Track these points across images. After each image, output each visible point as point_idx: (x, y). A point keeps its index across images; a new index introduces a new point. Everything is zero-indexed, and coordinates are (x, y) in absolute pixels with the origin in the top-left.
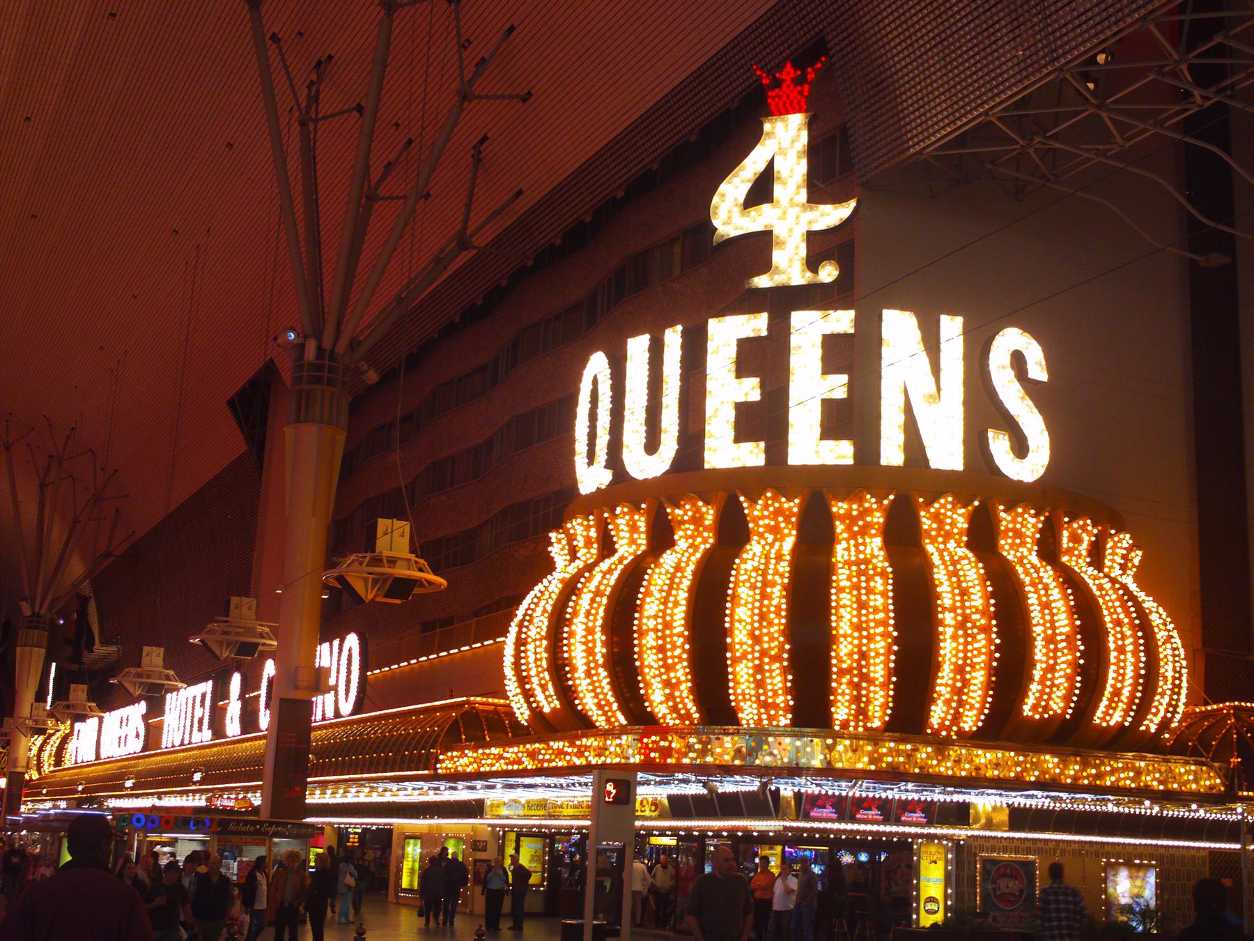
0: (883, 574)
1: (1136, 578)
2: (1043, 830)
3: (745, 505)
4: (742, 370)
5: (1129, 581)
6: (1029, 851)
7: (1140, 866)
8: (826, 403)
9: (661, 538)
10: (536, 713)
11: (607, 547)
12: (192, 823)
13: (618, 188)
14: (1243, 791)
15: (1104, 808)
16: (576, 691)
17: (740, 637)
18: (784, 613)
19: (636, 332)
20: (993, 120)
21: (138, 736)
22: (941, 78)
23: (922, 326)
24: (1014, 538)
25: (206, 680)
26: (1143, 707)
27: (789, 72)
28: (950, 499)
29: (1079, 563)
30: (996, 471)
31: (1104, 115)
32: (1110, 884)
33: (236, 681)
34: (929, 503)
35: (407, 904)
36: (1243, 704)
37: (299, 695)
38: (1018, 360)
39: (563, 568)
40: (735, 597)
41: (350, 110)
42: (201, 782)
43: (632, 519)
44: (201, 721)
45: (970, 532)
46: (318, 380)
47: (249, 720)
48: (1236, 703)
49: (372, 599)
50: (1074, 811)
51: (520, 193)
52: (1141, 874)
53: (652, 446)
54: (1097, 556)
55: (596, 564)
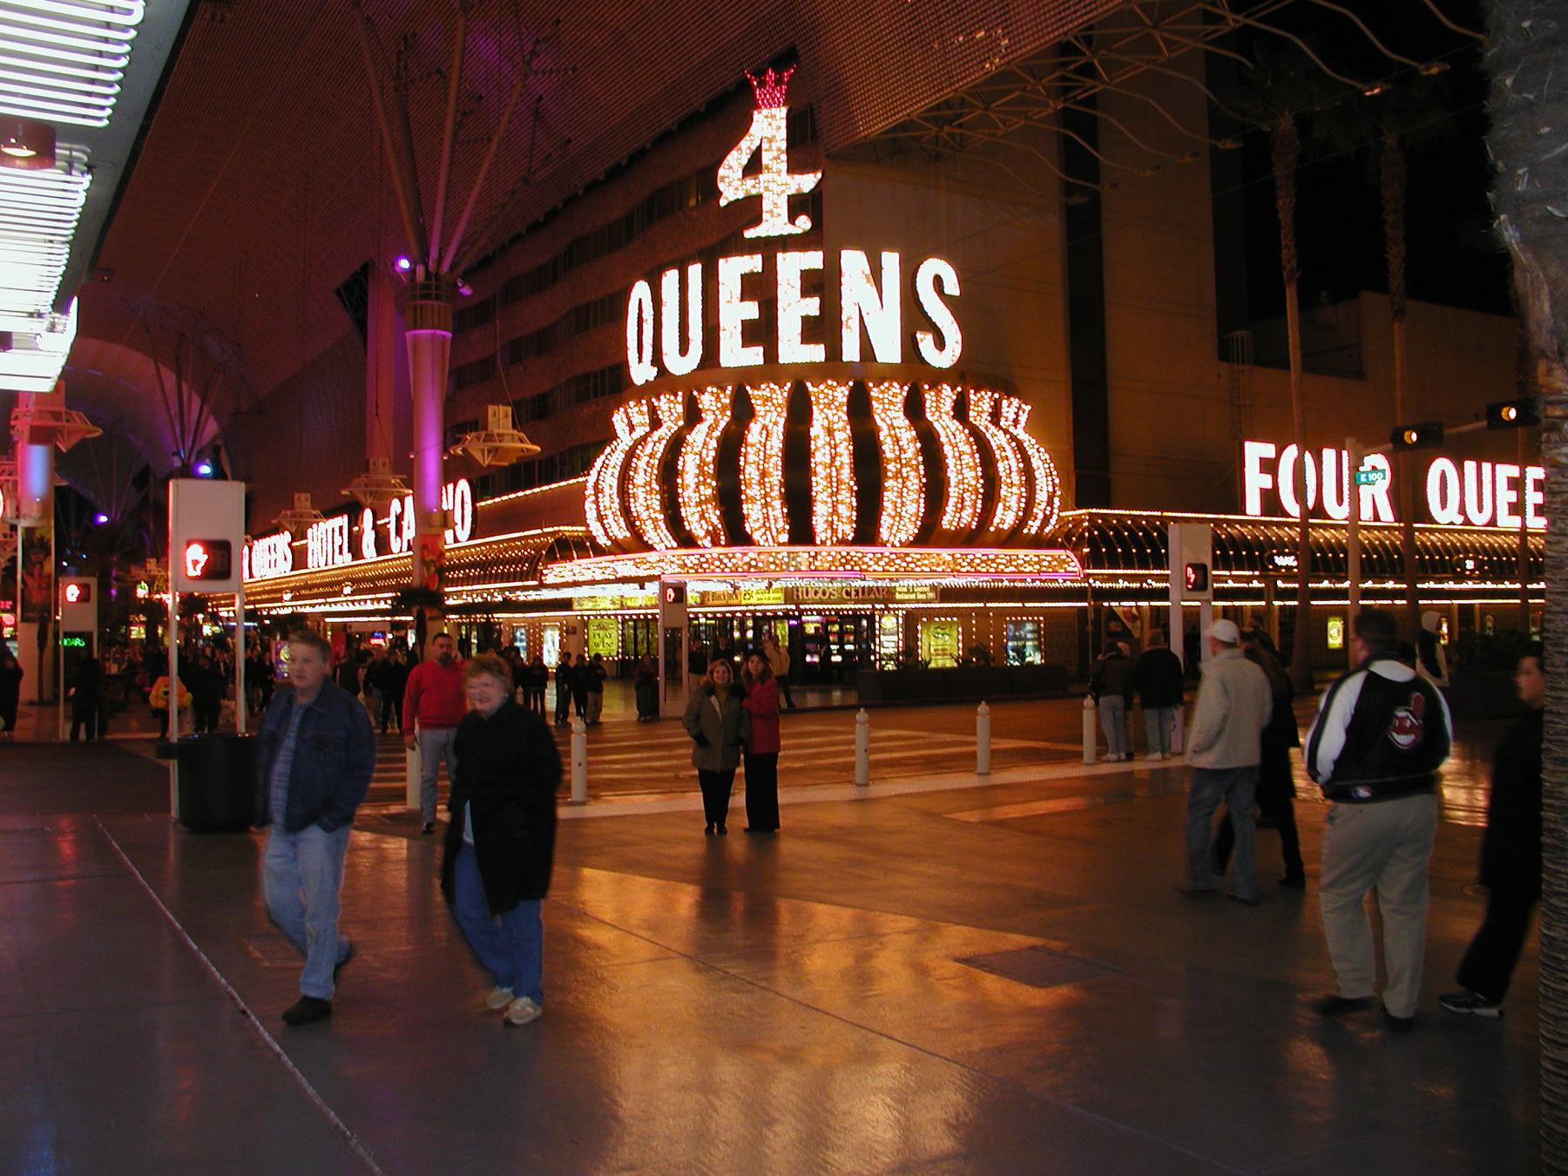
1: (1025, 429)
5: (1020, 433)
10: (615, 541)
11: (656, 423)
18: (780, 468)
22: (878, 86)
25: (341, 514)
26: (1027, 512)
29: (980, 419)
33: (368, 515)
37: (434, 531)
38: (938, 282)
39: (625, 440)
42: (353, 593)
44: (341, 547)
46: (427, 297)
47: (382, 545)
49: (489, 465)
53: (684, 350)
54: (995, 416)
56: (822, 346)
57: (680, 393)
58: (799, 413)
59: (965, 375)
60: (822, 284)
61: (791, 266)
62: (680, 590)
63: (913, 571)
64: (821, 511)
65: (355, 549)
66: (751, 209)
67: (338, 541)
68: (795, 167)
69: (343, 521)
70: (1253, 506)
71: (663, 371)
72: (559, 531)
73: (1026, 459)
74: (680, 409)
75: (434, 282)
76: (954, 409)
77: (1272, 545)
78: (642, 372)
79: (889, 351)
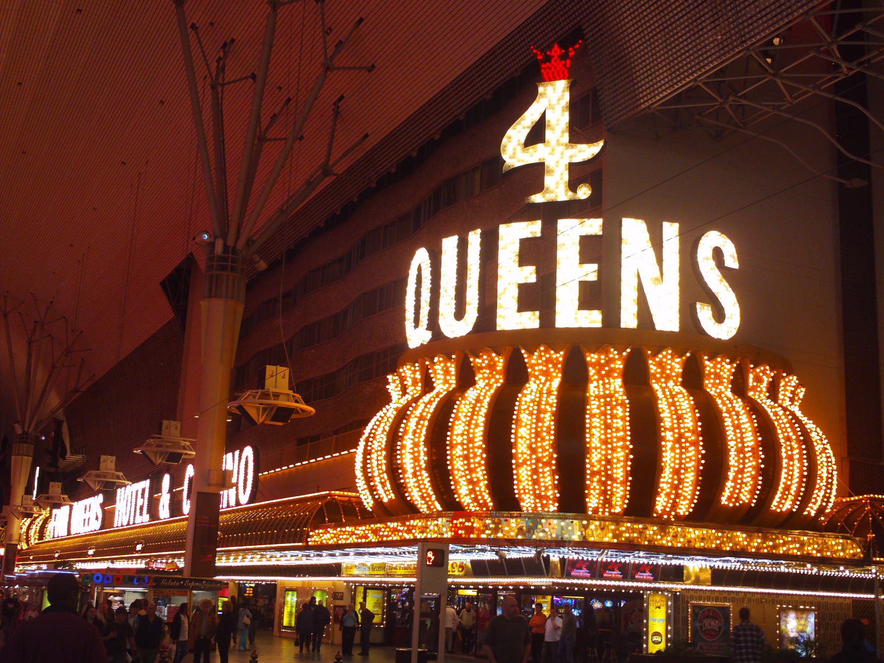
0: (622, 404)
1: (801, 407)
2: (735, 585)
3: (525, 356)
4: (523, 261)
5: (796, 409)
6: (725, 600)
7: (804, 610)
8: (582, 284)
9: (466, 379)
10: (378, 502)
11: (428, 385)
12: (135, 580)
13: (435, 132)
14: (876, 557)
15: (778, 569)
16: (406, 487)
17: (521, 448)
18: (552, 432)
19: (448, 234)
20: (700, 84)
21: (97, 518)
22: (663, 55)
23: (650, 230)
24: (715, 379)
25: (145, 479)
26: (805, 498)
27: (556, 51)
28: (670, 352)
29: (761, 397)
30: (702, 332)
31: (779, 81)
32: (782, 623)
33: (166, 480)
34: (655, 355)
35: (287, 637)
36: (876, 496)
37: (211, 490)
38: (718, 254)
39: (397, 400)
40: (518, 421)
41: (247, 78)
42: (142, 551)
43: (445, 366)
44: (141, 508)
45: (684, 375)
46: (224, 268)
47: (175, 507)
48: (872, 495)
49: (263, 422)
50: (757, 571)
51: (366, 136)
52: (804, 616)
53: (460, 314)
54: (773, 391)
55: (420, 397)
73: (805, 433)
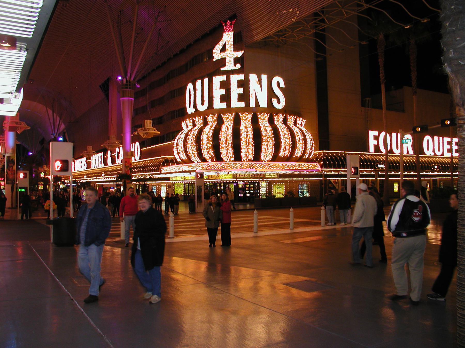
1: (304, 127)
5: (302, 128)
10: (182, 160)
11: (194, 125)
18: (231, 138)
22: (260, 25)
25: (101, 152)
26: (305, 152)
29: (291, 124)
33: (109, 152)
37: (129, 157)
38: (278, 83)
39: (185, 130)
42: (105, 176)
44: (101, 162)
46: (127, 88)
49: (145, 138)
53: (203, 104)
54: (295, 123)
56: (244, 102)
57: (202, 116)
58: (237, 122)
59: (286, 111)
60: (244, 84)
61: (235, 79)
62: (202, 175)
63: (271, 169)
64: (243, 151)
65: (105, 162)
66: (223, 62)
67: (100, 160)
68: (236, 50)
69: (102, 154)
70: (372, 150)
71: (196, 110)
72: (166, 157)
74: (202, 121)
75: (129, 84)
76: (283, 121)
77: (377, 161)
78: (190, 110)
79: (264, 104)
